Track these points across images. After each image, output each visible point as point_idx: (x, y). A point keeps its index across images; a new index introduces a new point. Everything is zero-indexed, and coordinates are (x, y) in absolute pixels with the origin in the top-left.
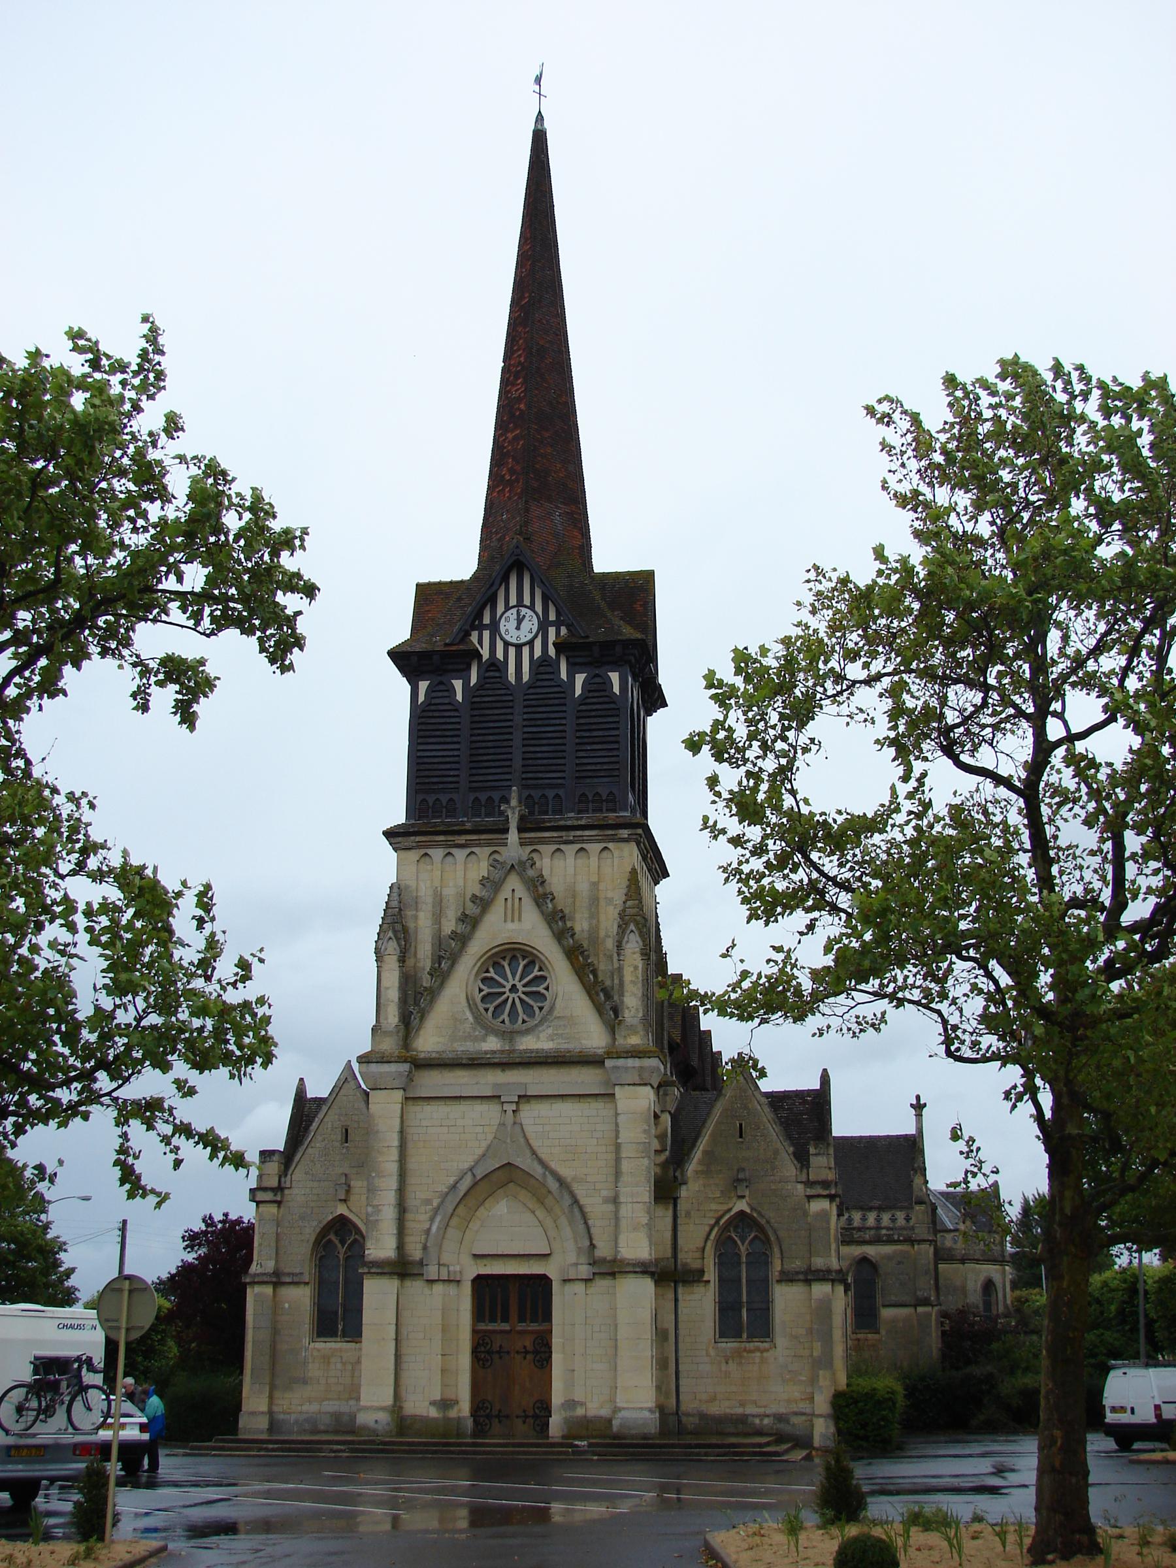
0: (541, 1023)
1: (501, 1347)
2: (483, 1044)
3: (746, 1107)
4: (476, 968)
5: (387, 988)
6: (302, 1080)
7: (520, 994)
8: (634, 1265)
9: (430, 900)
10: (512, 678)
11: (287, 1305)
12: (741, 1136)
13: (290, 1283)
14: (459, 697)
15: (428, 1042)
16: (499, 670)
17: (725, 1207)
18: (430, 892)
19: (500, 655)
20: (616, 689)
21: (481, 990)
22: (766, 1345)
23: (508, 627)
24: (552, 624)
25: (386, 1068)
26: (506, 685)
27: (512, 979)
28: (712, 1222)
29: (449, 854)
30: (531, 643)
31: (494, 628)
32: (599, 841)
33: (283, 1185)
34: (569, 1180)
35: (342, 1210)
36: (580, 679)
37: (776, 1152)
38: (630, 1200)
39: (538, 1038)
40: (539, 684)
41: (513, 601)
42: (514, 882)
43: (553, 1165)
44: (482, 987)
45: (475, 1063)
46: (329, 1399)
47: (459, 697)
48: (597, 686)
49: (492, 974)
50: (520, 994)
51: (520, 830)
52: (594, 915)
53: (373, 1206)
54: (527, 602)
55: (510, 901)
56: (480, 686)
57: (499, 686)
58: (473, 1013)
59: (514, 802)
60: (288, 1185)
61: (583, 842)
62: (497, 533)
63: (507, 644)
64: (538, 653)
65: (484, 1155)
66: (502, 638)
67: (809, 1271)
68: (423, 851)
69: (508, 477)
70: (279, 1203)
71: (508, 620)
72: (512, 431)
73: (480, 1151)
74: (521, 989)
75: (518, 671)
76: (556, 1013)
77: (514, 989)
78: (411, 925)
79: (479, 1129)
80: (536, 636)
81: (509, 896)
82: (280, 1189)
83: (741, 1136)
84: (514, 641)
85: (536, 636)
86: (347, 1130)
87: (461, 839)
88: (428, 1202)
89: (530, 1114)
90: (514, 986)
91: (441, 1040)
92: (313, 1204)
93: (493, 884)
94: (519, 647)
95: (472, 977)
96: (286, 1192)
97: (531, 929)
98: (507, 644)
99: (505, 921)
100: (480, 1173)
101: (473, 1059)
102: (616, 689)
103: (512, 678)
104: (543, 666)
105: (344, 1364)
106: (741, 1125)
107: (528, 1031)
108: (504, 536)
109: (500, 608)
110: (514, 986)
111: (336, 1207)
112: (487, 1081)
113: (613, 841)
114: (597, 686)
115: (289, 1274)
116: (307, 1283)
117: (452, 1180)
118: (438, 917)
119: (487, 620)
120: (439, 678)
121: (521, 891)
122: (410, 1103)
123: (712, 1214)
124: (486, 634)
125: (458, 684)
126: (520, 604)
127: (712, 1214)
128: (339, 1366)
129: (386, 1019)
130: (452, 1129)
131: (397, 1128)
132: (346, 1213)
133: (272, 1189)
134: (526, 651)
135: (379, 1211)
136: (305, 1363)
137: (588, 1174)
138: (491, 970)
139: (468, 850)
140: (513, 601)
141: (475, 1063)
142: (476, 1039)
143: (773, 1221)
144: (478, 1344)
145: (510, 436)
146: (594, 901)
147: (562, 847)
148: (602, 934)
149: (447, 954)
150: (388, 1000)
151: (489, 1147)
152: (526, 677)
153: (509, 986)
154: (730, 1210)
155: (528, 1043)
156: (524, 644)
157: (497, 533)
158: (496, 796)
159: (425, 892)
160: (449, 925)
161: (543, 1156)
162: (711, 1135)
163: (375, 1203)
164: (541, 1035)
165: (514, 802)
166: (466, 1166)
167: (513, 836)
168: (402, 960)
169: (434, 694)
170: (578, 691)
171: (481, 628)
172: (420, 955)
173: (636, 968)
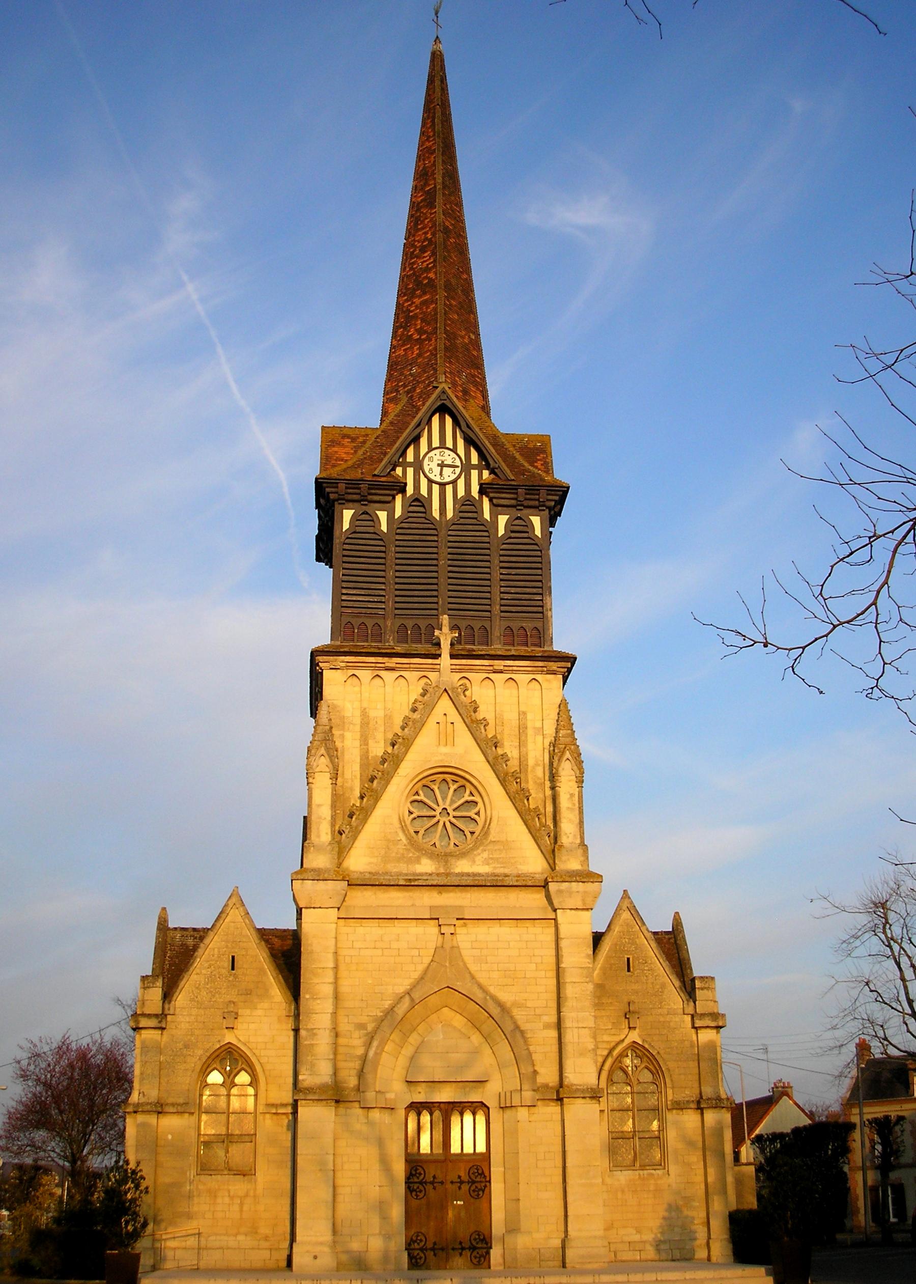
0: (475, 847)
1: (434, 1177)
3: (634, 943)
4: (407, 792)
5: (319, 806)
6: (164, 909)
7: (451, 818)
8: (583, 1091)
9: (358, 721)
10: (436, 514)
12: (629, 970)
14: (384, 528)
15: (359, 860)
16: (423, 506)
17: (617, 1039)
18: (358, 713)
19: (424, 491)
20: (538, 532)
21: (411, 813)
22: (660, 1172)
23: (431, 466)
24: (474, 467)
26: (431, 521)
27: (447, 800)
28: (605, 1053)
30: (454, 482)
31: (418, 466)
32: (528, 672)
33: (166, 1012)
34: (508, 1005)
35: (229, 1038)
36: (503, 520)
37: (663, 986)
38: (575, 1025)
39: (474, 862)
40: (462, 521)
41: (436, 443)
43: (492, 989)
44: (412, 809)
45: (411, 884)
46: (216, 1234)
47: (384, 528)
48: (519, 529)
49: (422, 797)
50: (451, 818)
51: (452, 656)
52: (522, 744)
54: (449, 444)
56: (403, 520)
57: (423, 520)
58: (406, 835)
59: (446, 629)
62: (405, 386)
63: (431, 482)
64: (461, 493)
65: (422, 978)
66: (426, 476)
68: (351, 672)
69: (416, 337)
71: (431, 459)
72: (420, 297)
73: (416, 975)
75: (440, 508)
76: (491, 838)
78: (338, 744)
79: (416, 952)
80: (459, 477)
83: (629, 970)
84: (438, 479)
85: (459, 477)
87: (392, 662)
89: (467, 938)
91: (374, 860)
92: (197, 1032)
93: (421, 710)
94: (443, 485)
95: (404, 798)
96: (169, 1018)
98: (431, 482)
100: (417, 996)
102: (538, 532)
103: (436, 514)
104: (467, 505)
105: (232, 1198)
106: (628, 959)
107: (463, 855)
108: (414, 389)
109: (424, 448)
111: (224, 1036)
112: (428, 899)
114: (519, 529)
115: (173, 1105)
117: (387, 1004)
118: (364, 740)
119: (410, 457)
123: (605, 1045)
124: (410, 471)
125: (383, 516)
126: (442, 446)
127: (605, 1045)
128: (227, 1200)
129: (319, 836)
130: (386, 952)
131: (332, 950)
132: (234, 1041)
133: (156, 1016)
134: (449, 488)
136: (190, 1196)
137: (531, 999)
138: (421, 792)
139: (397, 674)
140: (436, 443)
142: (410, 861)
143: (662, 1052)
144: (411, 1174)
145: (417, 301)
146: (522, 729)
147: (492, 676)
148: (531, 762)
149: (376, 778)
150: (320, 818)
151: (426, 971)
152: (450, 514)
153: (439, 810)
154: (623, 1040)
155: (462, 866)
156: (448, 483)
157: (405, 386)
158: (433, 622)
160: (378, 749)
161: (481, 981)
162: (601, 969)
165: (446, 629)
166: (401, 989)
167: (445, 660)
168: (335, 777)
169: (358, 523)
171: (405, 465)
172: (348, 775)
173: (572, 795)
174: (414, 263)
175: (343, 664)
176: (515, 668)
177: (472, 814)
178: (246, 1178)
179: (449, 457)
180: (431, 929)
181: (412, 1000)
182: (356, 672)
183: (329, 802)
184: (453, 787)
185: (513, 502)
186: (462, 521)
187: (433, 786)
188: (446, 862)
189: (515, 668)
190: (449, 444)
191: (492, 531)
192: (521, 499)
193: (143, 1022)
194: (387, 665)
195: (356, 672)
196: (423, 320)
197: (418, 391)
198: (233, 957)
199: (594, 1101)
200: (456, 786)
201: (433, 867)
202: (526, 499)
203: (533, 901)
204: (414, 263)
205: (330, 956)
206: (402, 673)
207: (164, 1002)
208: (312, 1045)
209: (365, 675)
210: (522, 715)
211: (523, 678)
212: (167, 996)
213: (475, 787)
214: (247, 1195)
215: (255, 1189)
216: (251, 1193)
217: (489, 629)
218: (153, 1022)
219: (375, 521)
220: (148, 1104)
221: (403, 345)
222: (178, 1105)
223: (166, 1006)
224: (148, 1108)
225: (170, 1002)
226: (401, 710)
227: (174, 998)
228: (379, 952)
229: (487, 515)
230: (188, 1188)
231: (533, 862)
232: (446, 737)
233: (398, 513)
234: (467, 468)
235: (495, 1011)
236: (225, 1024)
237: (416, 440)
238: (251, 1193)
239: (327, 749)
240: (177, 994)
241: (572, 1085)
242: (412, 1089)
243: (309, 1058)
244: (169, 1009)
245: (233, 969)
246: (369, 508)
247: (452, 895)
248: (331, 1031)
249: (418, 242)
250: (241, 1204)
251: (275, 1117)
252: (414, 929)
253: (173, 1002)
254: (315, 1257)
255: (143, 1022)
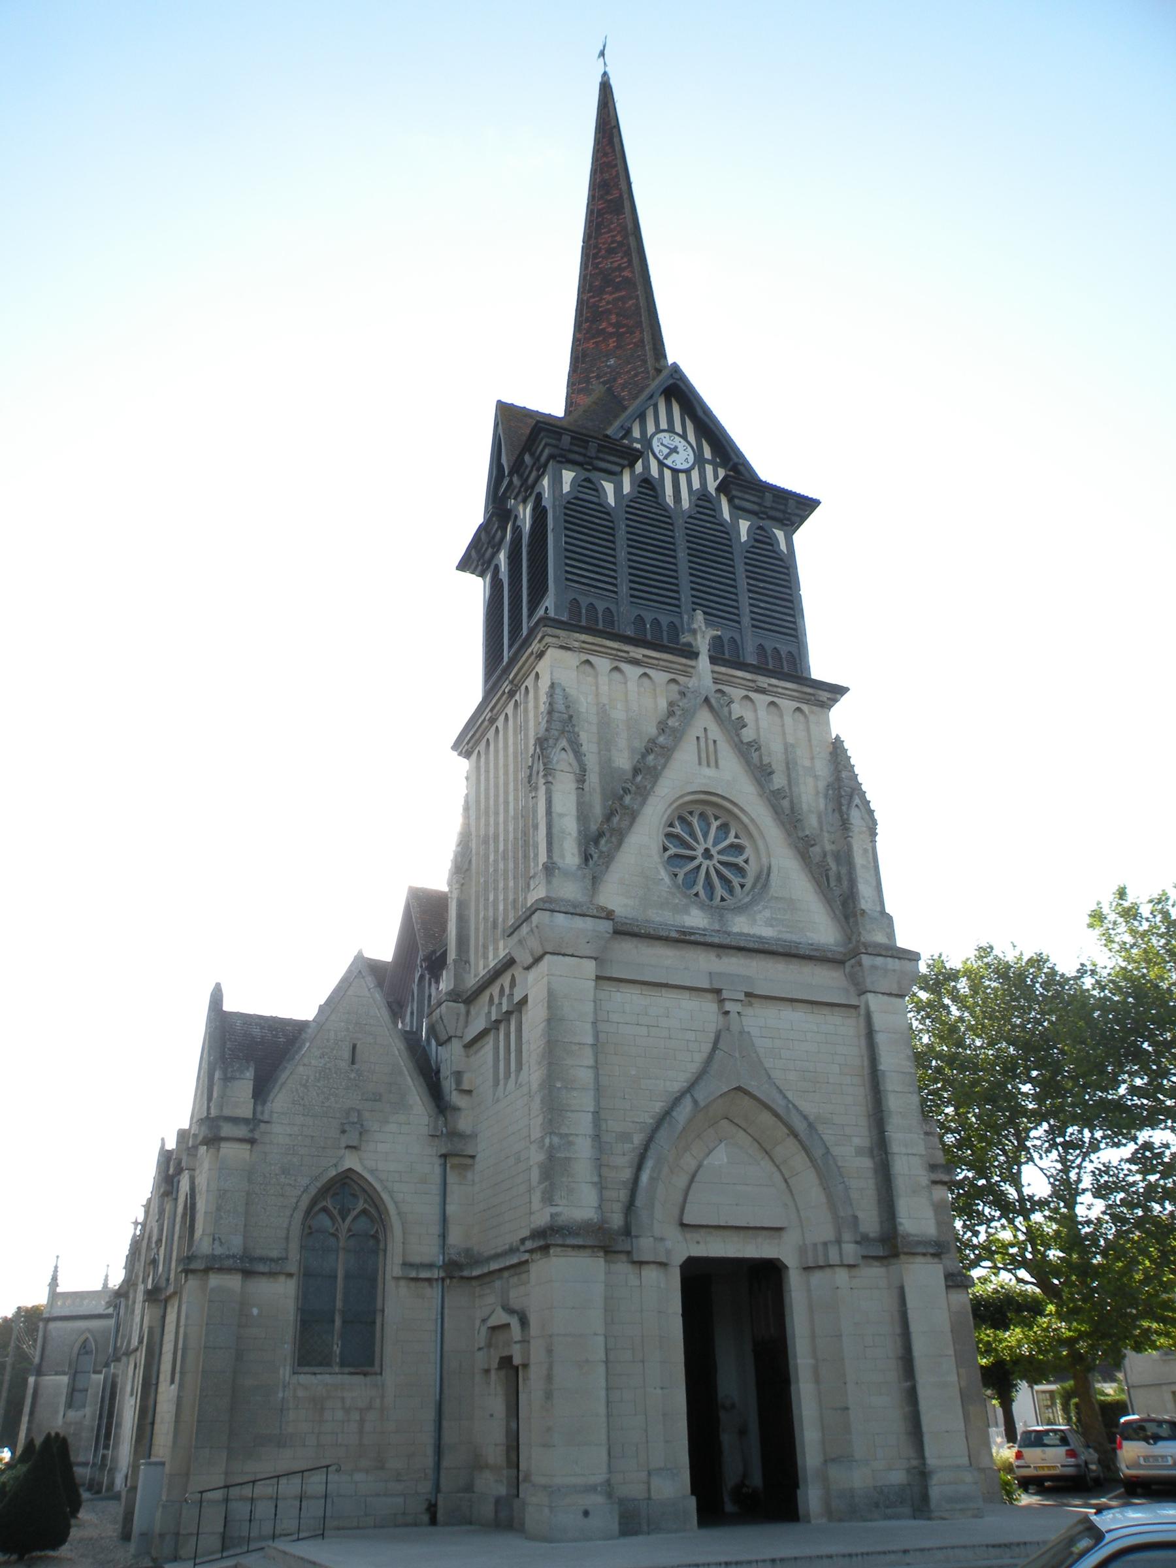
0: (753, 902)
2: (686, 918)
5: (561, 815)
7: (715, 861)
11: (255, 1311)
13: (263, 1274)
19: (654, 471)
24: (709, 462)
25: (579, 922)
26: (664, 507)
29: (616, 669)
32: (793, 698)
35: (351, 1162)
36: (744, 526)
38: (904, 1150)
40: (698, 516)
42: (704, 720)
43: (789, 1095)
45: (685, 940)
47: (611, 500)
49: (678, 830)
53: (561, 1136)
55: (702, 740)
60: (266, 1117)
61: (776, 694)
64: (696, 485)
67: (247, 1274)
68: (585, 657)
70: (252, 1142)
72: (611, 293)
74: (716, 857)
75: (679, 496)
77: (707, 854)
79: (691, 1036)
81: (702, 735)
82: (254, 1122)
86: (354, 1047)
87: (638, 653)
88: (625, 1137)
89: (759, 1022)
90: (707, 850)
97: (730, 778)
99: (700, 764)
101: (684, 933)
103: (670, 500)
104: (702, 498)
108: (615, 380)
110: (707, 850)
112: (700, 966)
113: (807, 702)
116: (290, 1275)
120: (587, 474)
121: (715, 732)
122: (606, 985)
125: (609, 487)
128: (340, 1415)
129: (563, 857)
131: (590, 1018)
132: (358, 1168)
133: (246, 1121)
135: (570, 1143)
139: (641, 671)
141: (685, 940)
147: (752, 695)
152: (685, 504)
155: (741, 925)
157: (598, 377)
159: (585, 704)
160: (623, 761)
163: (564, 1130)
164: (758, 917)
170: (744, 538)
174: (599, 263)
175: (576, 644)
176: (780, 690)
177: (739, 860)
178: (368, 1378)
179: (678, 442)
180: (708, 1007)
181: (695, 1102)
182: (592, 658)
183: (574, 812)
184: (715, 824)
185: (756, 508)
186: (698, 516)
187: (690, 818)
188: (721, 916)
189: (780, 690)
190: (679, 429)
191: (734, 536)
192: (768, 504)
193: (227, 1130)
194: (632, 654)
195: (592, 658)
196: (618, 315)
197: (620, 381)
198: (354, 1047)
199: (936, 1260)
200: (718, 823)
201: (706, 921)
202: (772, 508)
203: (825, 982)
204: (599, 263)
205: (588, 1027)
206: (648, 671)
207: (255, 1104)
208: (568, 1159)
209: (603, 664)
210: (788, 748)
211: (787, 705)
212: (260, 1092)
213: (746, 827)
214: (370, 1407)
215: (383, 1397)
216: (378, 1403)
217: (739, 643)
218: (242, 1131)
219: (598, 490)
220: (228, 1257)
221: (593, 337)
222: (272, 1260)
223: (259, 1108)
224: (229, 1263)
225: (264, 1103)
226: (749, 661)
227: (271, 1098)
228: (643, 1031)
229: (726, 515)
230: (280, 1395)
231: (822, 929)
232: (709, 758)
233: (627, 488)
234: (700, 460)
235: (800, 1126)
236: (344, 1141)
237: (642, 417)
238: (378, 1403)
239: (571, 742)
240: (275, 1090)
241: (908, 1235)
242: (688, 1236)
243: (564, 1179)
244: (262, 1113)
245: (353, 1062)
246: (594, 475)
247: (734, 960)
248: (593, 1140)
249: (604, 244)
250: (362, 1421)
251: (412, 1284)
252: (688, 1005)
253: (269, 1104)
254: (586, 1513)
255: (227, 1130)
